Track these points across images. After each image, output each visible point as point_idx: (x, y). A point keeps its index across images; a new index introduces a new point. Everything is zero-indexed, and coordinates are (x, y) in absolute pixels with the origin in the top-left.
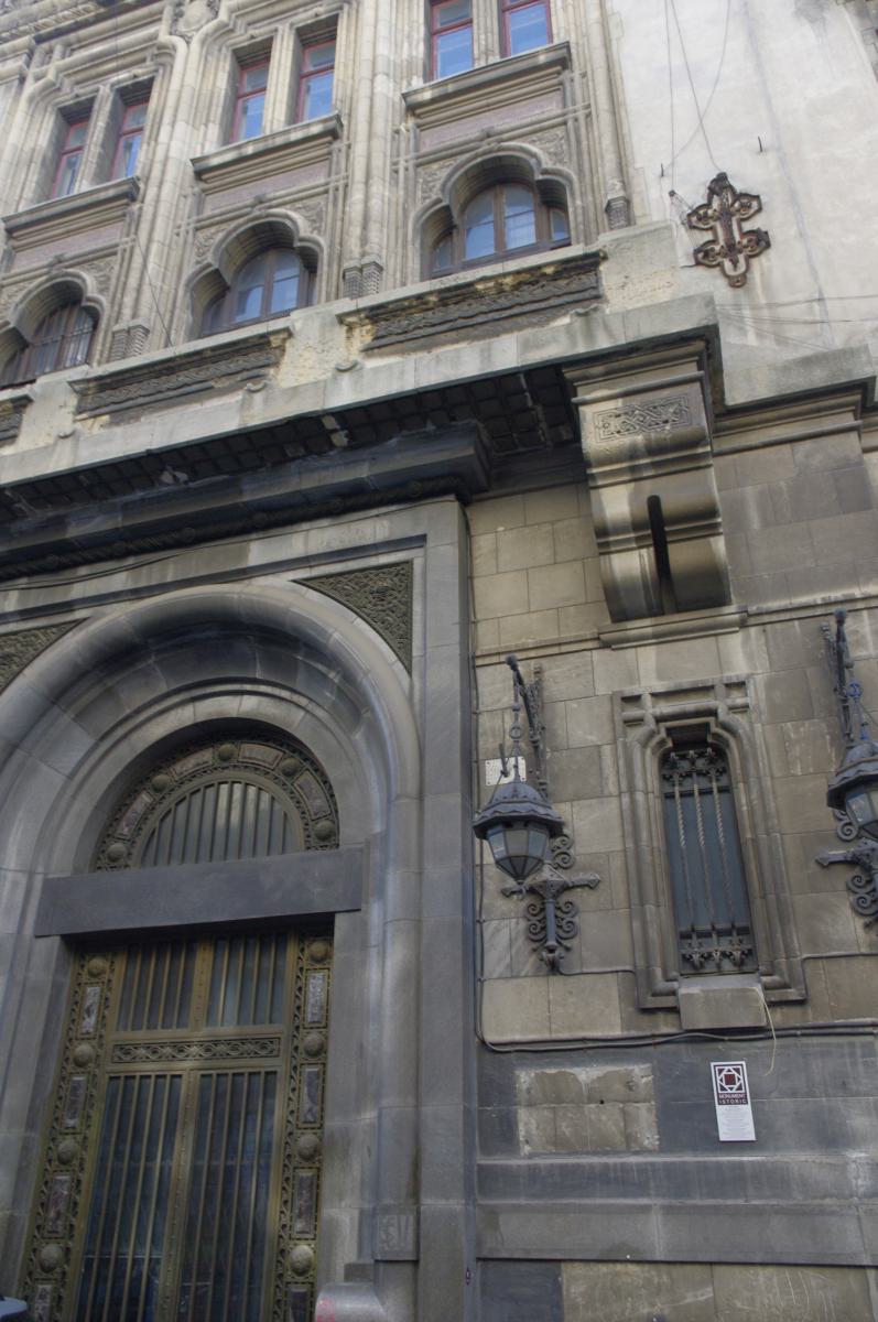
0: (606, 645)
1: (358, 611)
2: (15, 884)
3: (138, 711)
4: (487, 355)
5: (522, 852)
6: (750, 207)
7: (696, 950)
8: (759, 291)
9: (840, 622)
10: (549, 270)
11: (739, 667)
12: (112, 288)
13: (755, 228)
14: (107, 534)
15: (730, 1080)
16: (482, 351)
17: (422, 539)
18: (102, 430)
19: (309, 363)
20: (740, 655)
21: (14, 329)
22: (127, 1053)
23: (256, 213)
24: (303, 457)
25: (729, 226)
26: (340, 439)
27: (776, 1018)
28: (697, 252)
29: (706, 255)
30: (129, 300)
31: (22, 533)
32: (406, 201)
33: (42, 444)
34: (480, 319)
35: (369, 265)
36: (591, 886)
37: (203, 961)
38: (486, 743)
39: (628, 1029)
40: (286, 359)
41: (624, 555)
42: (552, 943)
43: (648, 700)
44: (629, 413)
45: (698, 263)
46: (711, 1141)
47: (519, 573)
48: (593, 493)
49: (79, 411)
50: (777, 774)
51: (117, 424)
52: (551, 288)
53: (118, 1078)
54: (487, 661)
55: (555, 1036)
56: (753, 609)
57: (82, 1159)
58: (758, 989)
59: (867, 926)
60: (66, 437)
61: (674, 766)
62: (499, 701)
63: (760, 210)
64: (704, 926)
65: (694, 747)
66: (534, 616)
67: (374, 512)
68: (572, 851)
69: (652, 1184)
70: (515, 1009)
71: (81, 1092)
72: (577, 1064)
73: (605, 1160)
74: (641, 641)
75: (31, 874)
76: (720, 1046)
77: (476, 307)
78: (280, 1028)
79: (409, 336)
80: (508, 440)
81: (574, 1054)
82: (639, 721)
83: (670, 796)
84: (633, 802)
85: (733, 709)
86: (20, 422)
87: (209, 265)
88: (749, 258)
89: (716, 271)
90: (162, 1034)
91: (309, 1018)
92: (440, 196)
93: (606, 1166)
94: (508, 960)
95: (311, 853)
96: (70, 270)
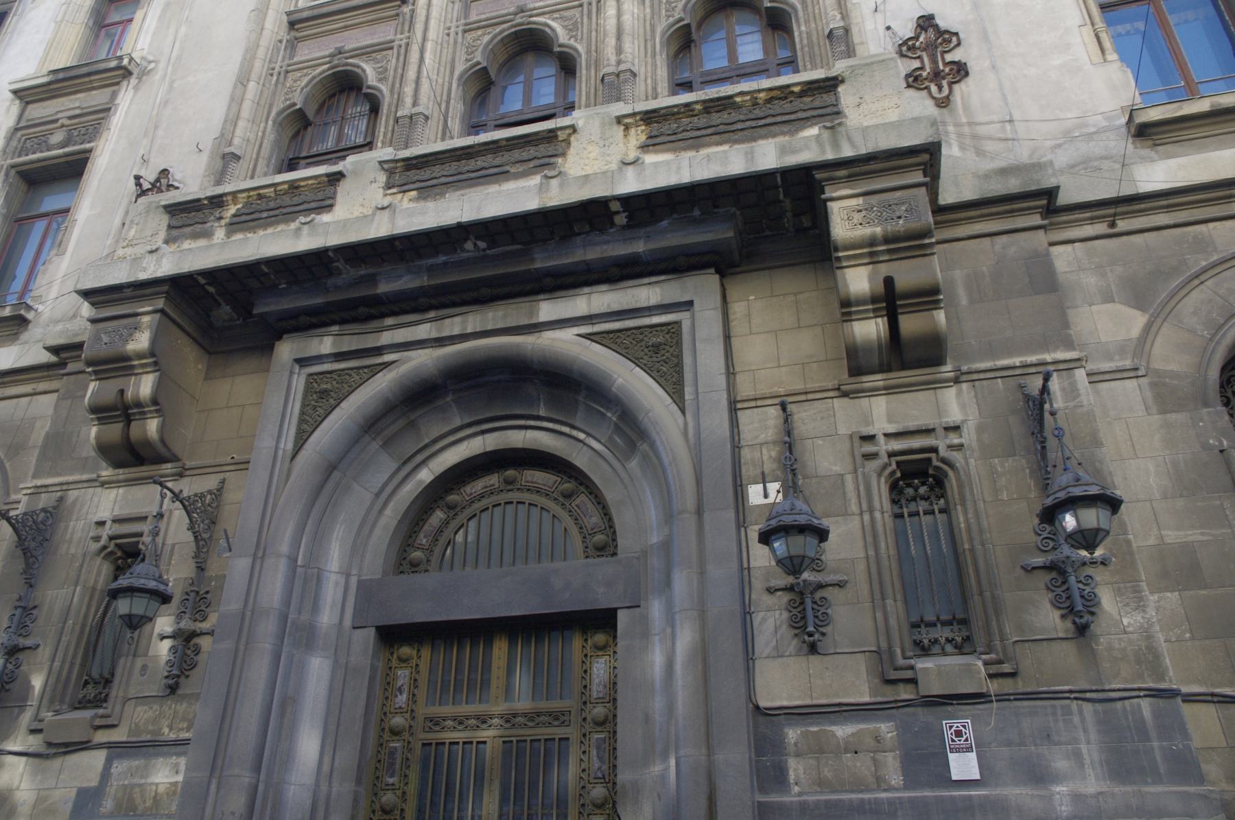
0: (845, 395)
1: (636, 361)
2: (337, 584)
3: (435, 441)
4: (750, 156)
5: (802, 553)
6: (950, 42)
7: (926, 636)
8: (961, 112)
9: (1047, 378)
10: (797, 89)
11: (954, 414)
12: (391, 79)
13: (956, 60)
14: (413, 290)
15: (959, 734)
16: (746, 153)
17: (690, 304)
18: (412, 205)
19: (592, 155)
20: (954, 404)
21: (300, 109)
22: (437, 724)
23: (518, 20)
24: (587, 233)
25: (934, 56)
26: (621, 220)
27: (993, 687)
28: (907, 76)
29: (916, 79)
30: (409, 90)
31: (337, 288)
32: (652, 18)
33: (356, 214)
34: (739, 126)
35: (625, 71)
36: (840, 585)
37: (500, 649)
38: (747, 471)
39: (875, 696)
40: (572, 151)
41: (863, 322)
42: (811, 629)
43: (881, 439)
44: (869, 209)
45: (909, 86)
46: (943, 778)
47: (758, 337)
48: (838, 272)
49: (388, 186)
50: (988, 499)
51: (425, 199)
52: (798, 104)
53: (430, 744)
54: (746, 405)
55: (815, 702)
56: (965, 368)
57: (402, 810)
58: (980, 663)
59: (1063, 617)
60: (383, 208)
61: (901, 492)
62: (756, 437)
63: (959, 44)
64: (930, 617)
65: (918, 476)
66: (784, 369)
67: (646, 280)
68: (823, 557)
69: (900, 813)
70: (782, 681)
71: (399, 756)
72: (834, 723)
73: (860, 796)
74: (873, 392)
75: (348, 575)
76: (949, 708)
77: (735, 116)
78: (569, 703)
79: (679, 136)
80: (771, 226)
81: (831, 716)
82: (874, 456)
83: (899, 516)
84: (873, 519)
85: (951, 447)
86: (335, 193)
87: (478, 63)
88: (951, 84)
89: (925, 93)
90: (464, 709)
91: (595, 695)
92: (682, 15)
93: (862, 800)
94: (774, 643)
95: (590, 560)
96: (350, 61)
